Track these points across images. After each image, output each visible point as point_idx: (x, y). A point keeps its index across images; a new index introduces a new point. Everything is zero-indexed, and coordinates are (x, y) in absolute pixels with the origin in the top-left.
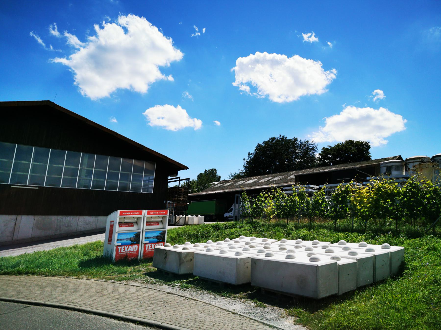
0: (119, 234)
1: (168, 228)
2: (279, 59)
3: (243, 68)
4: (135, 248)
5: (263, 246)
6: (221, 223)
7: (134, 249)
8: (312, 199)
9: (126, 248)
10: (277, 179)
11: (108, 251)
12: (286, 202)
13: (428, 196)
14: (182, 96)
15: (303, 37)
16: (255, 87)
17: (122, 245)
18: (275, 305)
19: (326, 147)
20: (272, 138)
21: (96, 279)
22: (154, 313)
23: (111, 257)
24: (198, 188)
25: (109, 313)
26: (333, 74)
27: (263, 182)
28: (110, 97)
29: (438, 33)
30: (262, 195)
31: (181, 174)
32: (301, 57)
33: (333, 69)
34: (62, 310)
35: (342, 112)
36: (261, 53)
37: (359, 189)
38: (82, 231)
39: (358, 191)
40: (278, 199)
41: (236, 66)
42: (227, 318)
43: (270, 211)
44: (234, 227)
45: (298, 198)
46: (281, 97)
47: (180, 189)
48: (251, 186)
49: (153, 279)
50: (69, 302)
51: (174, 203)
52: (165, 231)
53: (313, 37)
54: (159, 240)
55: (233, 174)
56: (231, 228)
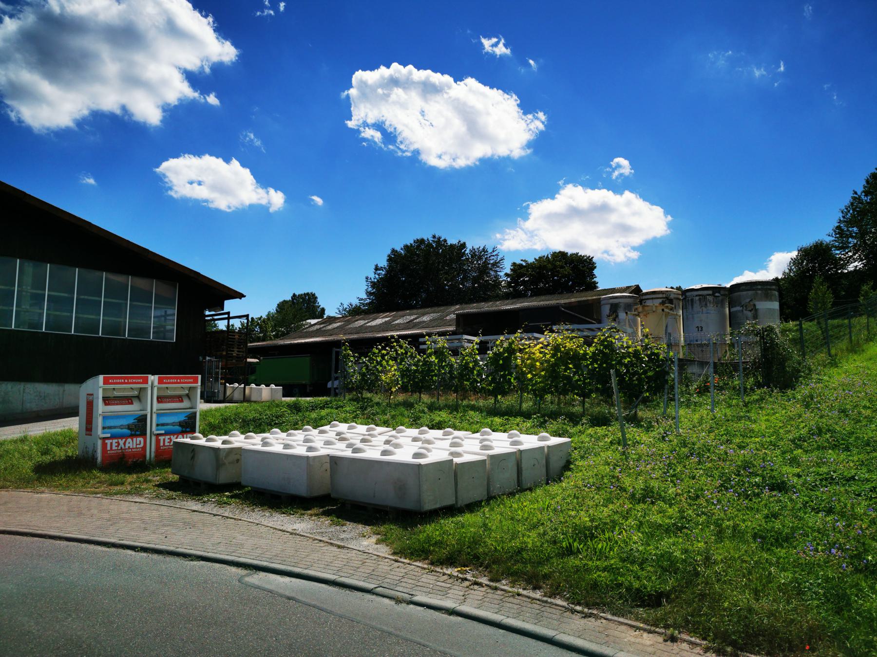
0: (104, 418)
1: (203, 406)
2: (437, 83)
3: (367, 91)
4: (138, 442)
5: (449, 442)
6: (303, 399)
7: (136, 445)
8: (458, 361)
9: (121, 442)
10: (426, 318)
11: (86, 448)
12: (416, 365)
13: (626, 361)
14: (241, 140)
15: (482, 44)
16: (391, 133)
17: (113, 437)
18: (359, 523)
19: (518, 262)
20: (418, 240)
21: (67, 493)
22: (166, 537)
23: (94, 458)
24: (276, 330)
25: (92, 538)
26: (538, 122)
27: (401, 324)
28: (76, 129)
29: (723, 62)
30: (377, 351)
31: (230, 306)
32: (479, 82)
33: (539, 113)
34: (10, 536)
35: (559, 194)
36: (402, 67)
37: (529, 347)
38: (34, 412)
39: (527, 350)
40: (402, 360)
41: (352, 87)
42: (280, 540)
43: (391, 380)
44: (327, 407)
45: (436, 359)
46: (442, 157)
47: (230, 335)
48: (379, 332)
49: (171, 493)
50: (22, 525)
51: (219, 361)
52: (195, 413)
53: (501, 45)
54: (184, 429)
55: (345, 306)
56: (322, 408)
